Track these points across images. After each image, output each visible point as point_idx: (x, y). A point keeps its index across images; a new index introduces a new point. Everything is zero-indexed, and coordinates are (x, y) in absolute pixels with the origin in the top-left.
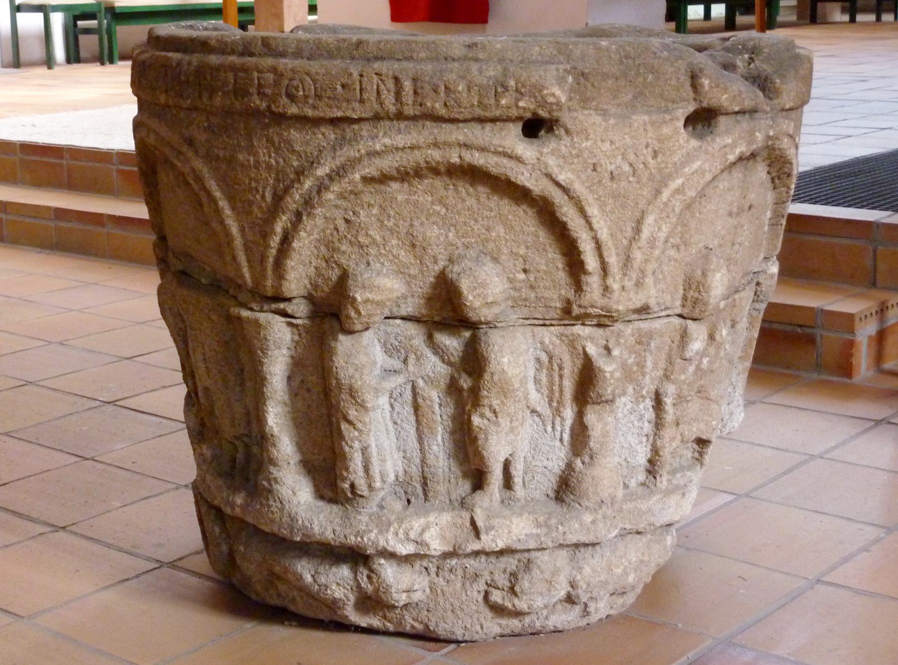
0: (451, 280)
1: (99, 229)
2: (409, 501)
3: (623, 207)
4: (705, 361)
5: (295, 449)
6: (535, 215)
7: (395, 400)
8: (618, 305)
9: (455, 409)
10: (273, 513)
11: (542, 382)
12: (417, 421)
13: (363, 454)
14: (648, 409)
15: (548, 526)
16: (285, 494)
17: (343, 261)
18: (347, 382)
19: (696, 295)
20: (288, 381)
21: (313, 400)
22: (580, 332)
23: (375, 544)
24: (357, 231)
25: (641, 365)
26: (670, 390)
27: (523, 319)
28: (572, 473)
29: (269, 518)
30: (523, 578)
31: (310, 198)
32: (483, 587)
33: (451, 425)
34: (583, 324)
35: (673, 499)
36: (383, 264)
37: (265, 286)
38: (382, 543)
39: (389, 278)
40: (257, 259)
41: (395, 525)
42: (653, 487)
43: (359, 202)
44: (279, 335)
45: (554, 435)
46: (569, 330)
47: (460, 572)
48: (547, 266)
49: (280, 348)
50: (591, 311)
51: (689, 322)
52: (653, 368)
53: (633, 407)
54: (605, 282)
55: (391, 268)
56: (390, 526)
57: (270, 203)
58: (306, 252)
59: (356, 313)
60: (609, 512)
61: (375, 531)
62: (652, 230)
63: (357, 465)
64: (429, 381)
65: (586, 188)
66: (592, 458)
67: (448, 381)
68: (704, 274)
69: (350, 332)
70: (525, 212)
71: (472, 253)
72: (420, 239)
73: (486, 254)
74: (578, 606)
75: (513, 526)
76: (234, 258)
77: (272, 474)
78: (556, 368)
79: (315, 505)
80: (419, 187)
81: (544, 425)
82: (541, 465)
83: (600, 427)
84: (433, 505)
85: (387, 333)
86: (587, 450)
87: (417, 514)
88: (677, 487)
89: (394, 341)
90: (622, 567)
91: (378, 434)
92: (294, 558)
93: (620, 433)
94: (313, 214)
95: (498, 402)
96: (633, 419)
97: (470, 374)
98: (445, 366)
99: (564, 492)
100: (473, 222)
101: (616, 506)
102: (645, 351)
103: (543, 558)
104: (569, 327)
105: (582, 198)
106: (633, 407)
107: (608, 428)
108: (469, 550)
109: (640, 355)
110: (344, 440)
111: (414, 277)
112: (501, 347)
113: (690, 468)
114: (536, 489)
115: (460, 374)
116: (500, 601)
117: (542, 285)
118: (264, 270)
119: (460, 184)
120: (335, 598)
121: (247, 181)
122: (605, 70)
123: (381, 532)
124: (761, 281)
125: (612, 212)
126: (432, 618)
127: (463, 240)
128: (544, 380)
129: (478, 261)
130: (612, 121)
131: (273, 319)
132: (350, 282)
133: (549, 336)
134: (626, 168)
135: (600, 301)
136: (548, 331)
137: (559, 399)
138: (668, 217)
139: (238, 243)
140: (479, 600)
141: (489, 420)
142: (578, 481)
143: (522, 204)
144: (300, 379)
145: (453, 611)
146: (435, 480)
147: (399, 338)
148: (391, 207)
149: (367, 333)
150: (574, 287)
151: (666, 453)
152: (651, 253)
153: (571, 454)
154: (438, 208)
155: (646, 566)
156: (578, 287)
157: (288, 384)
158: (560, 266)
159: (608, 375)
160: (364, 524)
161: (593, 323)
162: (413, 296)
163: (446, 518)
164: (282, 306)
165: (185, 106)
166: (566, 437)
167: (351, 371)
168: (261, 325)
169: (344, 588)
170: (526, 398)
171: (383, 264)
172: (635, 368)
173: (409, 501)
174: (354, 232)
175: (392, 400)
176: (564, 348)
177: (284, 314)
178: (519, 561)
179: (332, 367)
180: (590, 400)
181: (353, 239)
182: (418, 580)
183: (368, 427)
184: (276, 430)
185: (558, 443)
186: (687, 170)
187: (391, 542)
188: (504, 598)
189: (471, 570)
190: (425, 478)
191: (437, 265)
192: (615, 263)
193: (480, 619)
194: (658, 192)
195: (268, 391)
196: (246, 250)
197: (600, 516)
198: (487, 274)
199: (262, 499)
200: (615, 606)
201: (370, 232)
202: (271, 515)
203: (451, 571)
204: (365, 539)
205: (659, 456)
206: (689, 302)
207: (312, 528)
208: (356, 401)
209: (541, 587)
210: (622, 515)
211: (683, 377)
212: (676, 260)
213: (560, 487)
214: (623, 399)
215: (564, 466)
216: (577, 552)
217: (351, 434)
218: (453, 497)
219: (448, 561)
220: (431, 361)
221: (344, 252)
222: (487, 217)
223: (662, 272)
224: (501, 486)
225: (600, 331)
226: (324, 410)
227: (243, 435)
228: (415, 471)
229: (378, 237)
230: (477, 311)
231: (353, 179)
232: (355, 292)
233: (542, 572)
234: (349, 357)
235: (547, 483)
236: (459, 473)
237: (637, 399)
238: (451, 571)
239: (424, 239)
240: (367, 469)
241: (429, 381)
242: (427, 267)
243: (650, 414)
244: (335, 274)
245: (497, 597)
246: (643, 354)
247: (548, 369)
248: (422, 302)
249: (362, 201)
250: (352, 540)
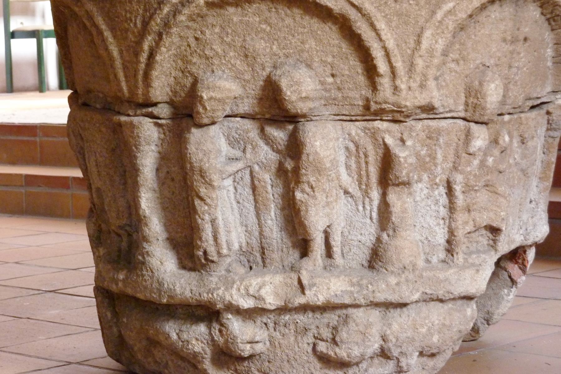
0: (275, 81)
1: (65, 191)
2: (251, 268)
3: (406, 23)
4: (490, 160)
5: (163, 228)
6: (338, 30)
7: (238, 183)
8: (406, 101)
9: (283, 188)
10: (145, 281)
11: (351, 168)
12: (256, 201)
13: (212, 225)
14: (442, 195)
15: (360, 285)
16: (154, 265)
17: (194, 70)
18: (197, 165)
19: (475, 101)
20: (156, 172)
21: (176, 187)
22: (379, 126)
23: (223, 299)
24: (204, 46)
25: (433, 157)
26: (459, 178)
27: (334, 115)
28: (380, 245)
29: (143, 285)
30: (342, 329)
31: (168, 21)
32: (311, 340)
33: (281, 203)
34: (381, 120)
35: (468, 273)
36: (224, 71)
37: (137, 94)
38: (228, 298)
39: (228, 81)
40: (131, 76)
41: (238, 283)
42: (451, 263)
43: (205, 23)
44: (148, 133)
45: (365, 214)
46: (370, 125)
47: (292, 327)
48: (350, 71)
49: (149, 144)
50: (384, 106)
51: (472, 124)
52: (443, 160)
53: (429, 193)
54: (394, 83)
55: (230, 74)
56: (234, 283)
57: (140, 28)
58: (167, 65)
59: (203, 109)
60: (411, 276)
61: (222, 289)
62: (431, 42)
63: (208, 235)
64: (264, 166)
65: (375, 7)
66: (395, 231)
67: (277, 166)
68: (481, 84)
69: (200, 126)
70: (330, 28)
71: (291, 60)
72: (251, 50)
73: (301, 62)
74: (392, 361)
75: (332, 284)
76: (116, 76)
77: (145, 248)
78: (362, 155)
79: (178, 273)
80: (249, 10)
81: (356, 205)
82: (355, 239)
83: (399, 204)
84: (270, 270)
85: (230, 128)
86: (391, 224)
87: (256, 276)
88: (473, 265)
89: (235, 135)
90: (426, 327)
91: (224, 209)
92: (164, 320)
93: (420, 214)
94: (170, 33)
95: (314, 179)
96: (430, 203)
97: (292, 158)
98: (274, 154)
99: (375, 261)
100: (291, 37)
101: (417, 272)
102: (435, 145)
103: (358, 314)
104: (370, 122)
105: (371, 15)
106: (429, 193)
107: (406, 205)
108: (296, 304)
109: (431, 148)
110: (198, 214)
111: (248, 82)
112: (314, 133)
113: (484, 252)
114: (353, 260)
115: (285, 159)
116: (325, 351)
117: (346, 86)
118: (136, 81)
119: (280, 7)
120: (195, 352)
121: (124, 14)
123: (227, 289)
124: (551, 110)
125: (397, 27)
126: (272, 368)
127: (284, 51)
128: (354, 166)
129: (295, 67)
131: (143, 120)
132: (199, 85)
133: (355, 129)
135: (392, 99)
136: (355, 125)
137: (367, 183)
138: (443, 32)
139: (118, 63)
140: (309, 351)
141: (308, 194)
142: (385, 251)
143: (328, 22)
144: (166, 171)
145: (288, 361)
146: (271, 249)
147: (239, 132)
148: (229, 26)
149: (213, 127)
150: (371, 88)
151: (460, 234)
152: (431, 61)
153: (379, 229)
154: (264, 26)
155: (448, 330)
156: (374, 87)
157: (156, 175)
158: (360, 71)
159: (402, 160)
160: (214, 283)
161: (389, 118)
162: (248, 97)
163: (278, 279)
164: (150, 110)
166: (375, 215)
167: (201, 155)
168: (134, 125)
169: (202, 342)
170: (338, 179)
171: (224, 71)
172: (428, 159)
173: (251, 268)
174: (202, 48)
175: (236, 184)
176: (368, 139)
177: (152, 116)
178: (339, 317)
179: (186, 154)
180: (390, 182)
181: (201, 53)
182: (259, 333)
183: (215, 202)
184: (147, 212)
185: (368, 221)
187: (235, 297)
188: (328, 348)
189: (300, 324)
190: (263, 248)
191: (265, 71)
192: (402, 68)
193: (311, 368)
194: (434, 13)
195: (141, 180)
196: (124, 69)
197: (403, 280)
198: (301, 75)
199: (138, 271)
200: (426, 368)
201: (214, 47)
202: (144, 283)
203: (285, 326)
204: (215, 295)
205: (455, 236)
206: (470, 107)
207: (175, 290)
208: (206, 181)
209: (358, 338)
210: (422, 280)
211: (469, 169)
212: (456, 72)
213: (372, 257)
214: (420, 185)
215: (374, 241)
216: (388, 313)
217: (203, 209)
218: (286, 263)
219: (283, 317)
220: (263, 150)
221: (195, 63)
222: (302, 33)
223: (444, 81)
224: (324, 255)
225: (395, 127)
226: (184, 195)
227: (126, 225)
228: (255, 243)
229: (219, 50)
230: (295, 104)
231: (199, 4)
232: (203, 92)
233: (357, 325)
234: (199, 145)
235: (363, 255)
236: (290, 244)
237: (431, 185)
238: (285, 326)
239: (254, 51)
240: (216, 239)
241: (264, 166)
242: (257, 73)
243: (444, 200)
244: (188, 82)
245: (322, 347)
246: (434, 147)
247: (356, 157)
248: (255, 102)
249: (206, 21)
250: (205, 297)
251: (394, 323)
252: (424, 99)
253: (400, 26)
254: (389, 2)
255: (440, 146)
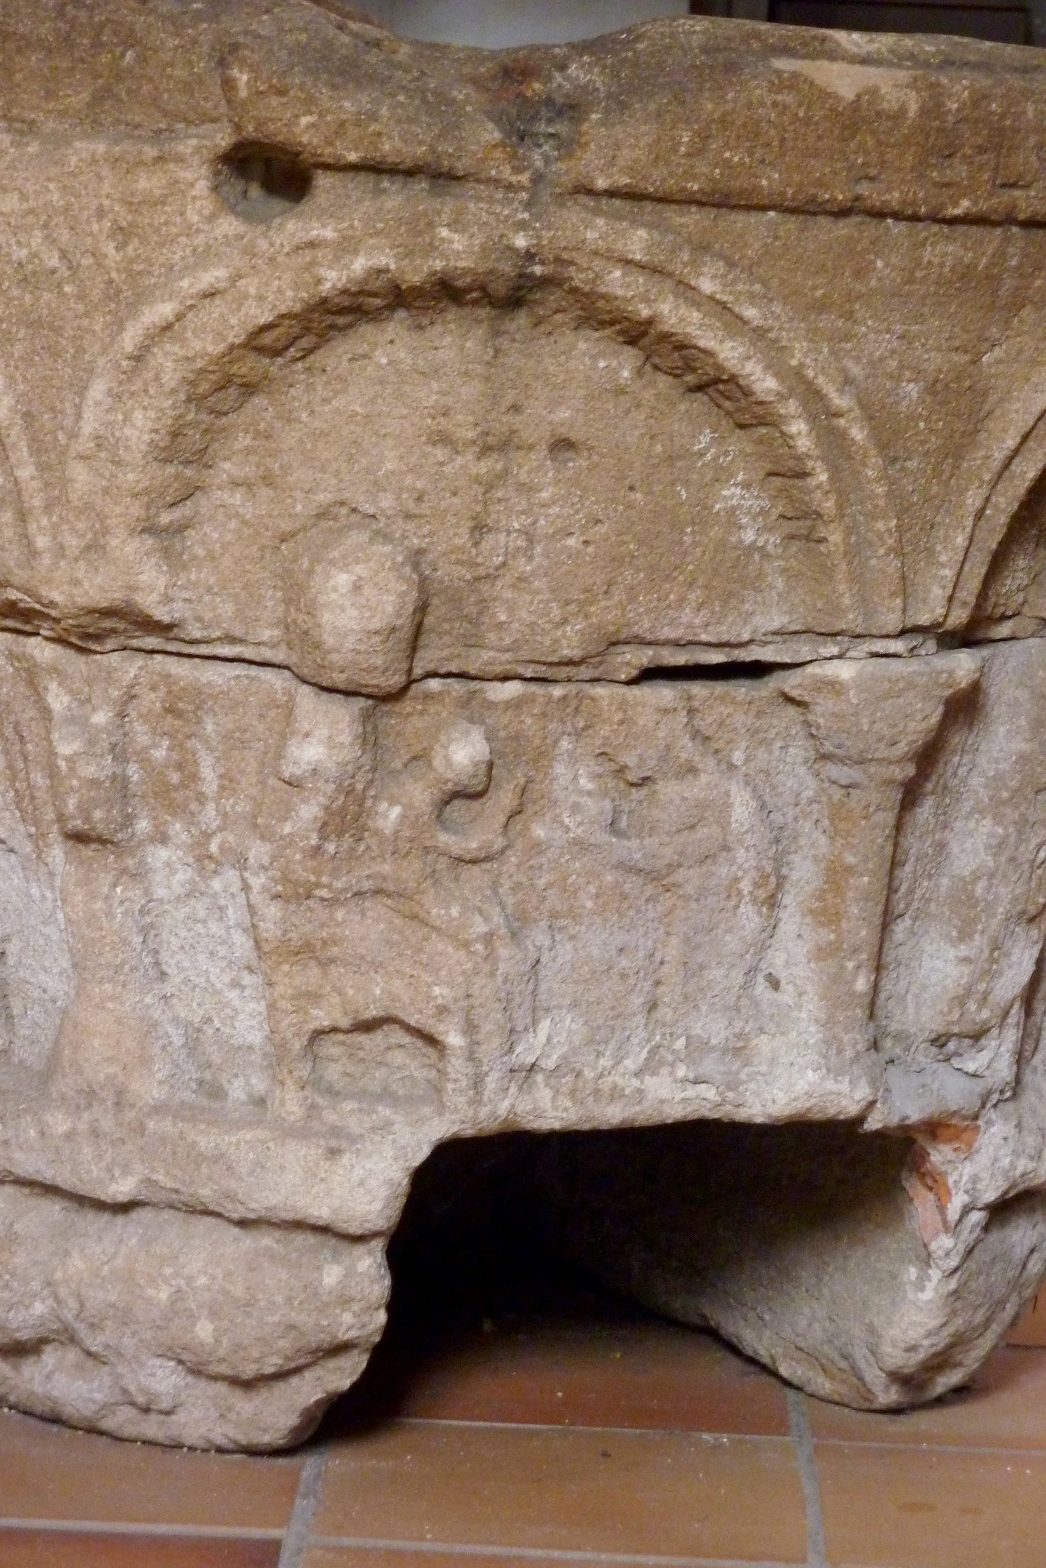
52: (222, 788)
101: (130, 1115)
122: (21, 29)
125: (28, 361)
130: (33, 148)
134: (53, 261)
165: (781, 227)
172: (175, 778)
186: (185, 283)
197: (82, 1127)
200: (232, 1416)
211: (287, 829)
237: (199, 859)
251: (75, 1254)
252: (102, 589)
253: (37, 358)
254: (7, 284)
255: (206, 742)
